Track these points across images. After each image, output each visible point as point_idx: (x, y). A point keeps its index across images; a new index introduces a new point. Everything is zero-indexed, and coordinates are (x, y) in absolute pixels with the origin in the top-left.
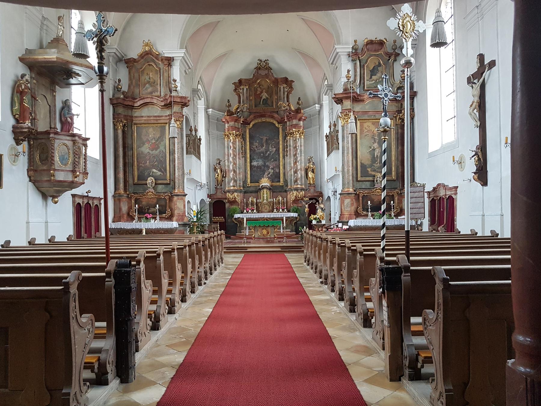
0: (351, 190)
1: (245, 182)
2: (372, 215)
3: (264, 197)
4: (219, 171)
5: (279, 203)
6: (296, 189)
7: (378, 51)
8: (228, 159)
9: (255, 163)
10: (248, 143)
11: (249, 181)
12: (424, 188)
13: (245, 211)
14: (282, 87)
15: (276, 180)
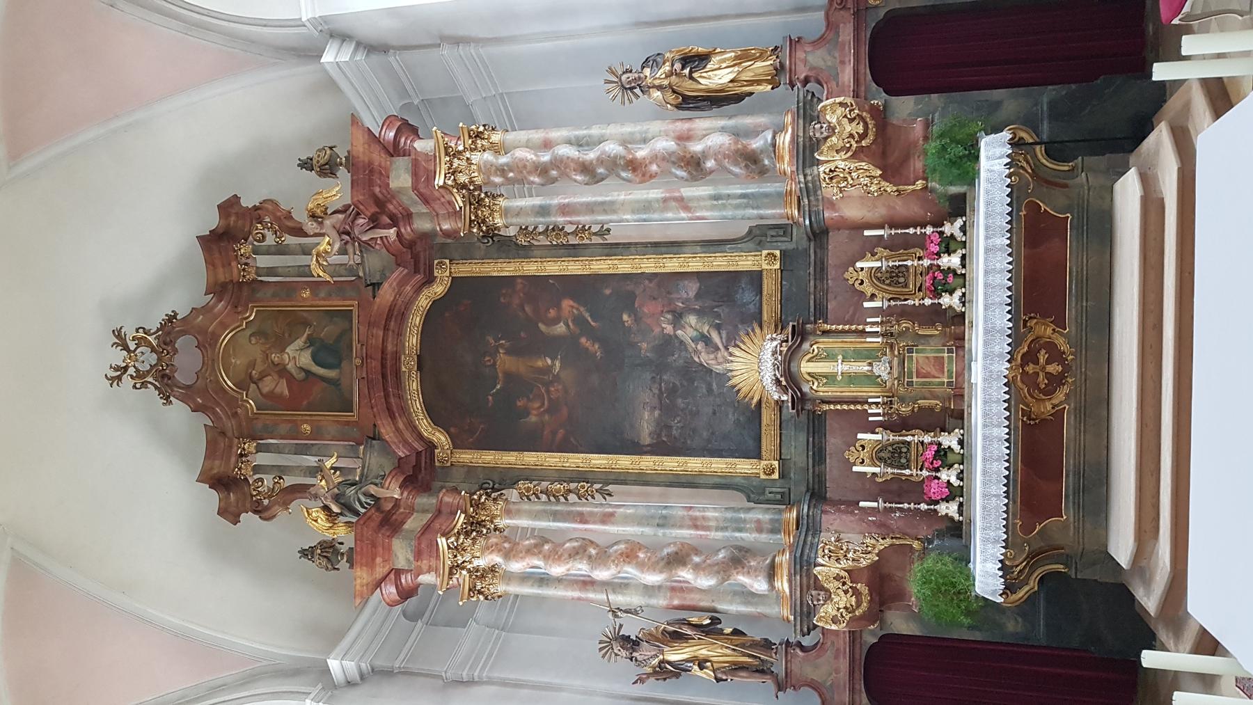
1: (753, 492)
3: (851, 379)
4: (675, 655)
5: (895, 277)
6: (807, 152)
8: (606, 585)
9: (646, 424)
10: (531, 458)
11: (744, 466)
13: (949, 509)
14: (263, 261)
15: (747, 296)
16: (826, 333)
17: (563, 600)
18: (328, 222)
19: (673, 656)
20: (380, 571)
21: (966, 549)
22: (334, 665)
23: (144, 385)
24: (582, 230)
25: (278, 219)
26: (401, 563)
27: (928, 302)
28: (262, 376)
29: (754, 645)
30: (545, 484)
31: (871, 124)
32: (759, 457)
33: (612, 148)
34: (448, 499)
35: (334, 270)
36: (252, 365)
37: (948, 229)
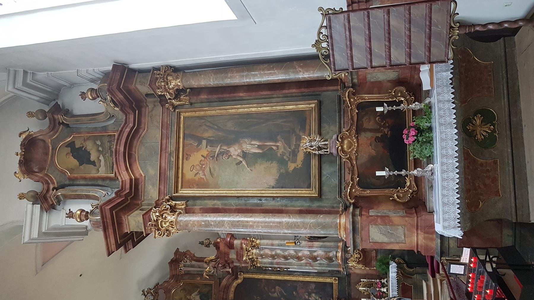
0: (344, 220)
2: (417, 164)
6: (345, 260)
7: (46, 147)
12: (335, 13)
25: (191, 257)
33: (292, 252)
37: (383, 281)
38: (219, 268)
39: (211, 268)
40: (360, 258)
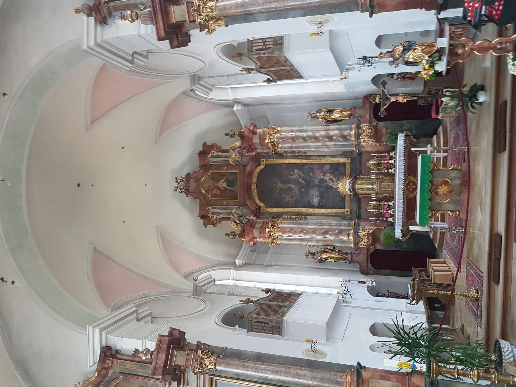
1: (343, 217)
3: (368, 189)
5: (379, 165)
8: (308, 240)
9: (316, 201)
10: (286, 210)
11: (341, 211)
13: (391, 219)
14: (212, 159)
15: (342, 169)
16: (362, 178)
17: (296, 244)
18: (236, 151)
19: (324, 256)
20: (251, 237)
21: (394, 228)
22: (237, 261)
23: (182, 192)
24: (300, 152)
26: (256, 235)
27: (386, 171)
28: (213, 189)
29: (344, 253)
30: (290, 216)
31: (373, 130)
32: (345, 208)
33: (310, 133)
34: (266, 220)
35: (235, 161)
36: (210, 186)
37: (391, 154)
38: (244, 153)
39: (237, 154)
40: (371, 133)
